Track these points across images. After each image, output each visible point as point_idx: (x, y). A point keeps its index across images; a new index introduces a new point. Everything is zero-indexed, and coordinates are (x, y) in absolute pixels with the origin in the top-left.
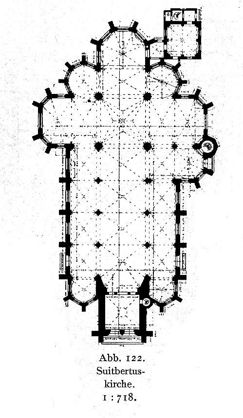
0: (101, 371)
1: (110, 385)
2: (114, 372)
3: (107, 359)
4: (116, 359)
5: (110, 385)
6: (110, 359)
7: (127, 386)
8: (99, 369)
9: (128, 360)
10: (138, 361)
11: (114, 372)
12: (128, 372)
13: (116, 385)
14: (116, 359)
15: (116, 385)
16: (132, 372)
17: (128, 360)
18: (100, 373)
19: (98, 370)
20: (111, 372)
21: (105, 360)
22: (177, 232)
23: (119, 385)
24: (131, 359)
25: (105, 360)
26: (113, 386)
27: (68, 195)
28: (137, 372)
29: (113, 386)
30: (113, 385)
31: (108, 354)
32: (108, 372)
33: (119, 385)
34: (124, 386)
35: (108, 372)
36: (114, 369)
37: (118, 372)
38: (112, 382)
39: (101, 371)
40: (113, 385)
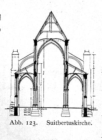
0: (49, 123)
1: (77, 123)
2: (57, 123)
3: (14, 123)
4: (20, 123)
5: (77, 123)
6: (16, 123)
7: (87, 124)
8: (48, 121)
9: (27, 124)
10: (30, 124)
11: (57, 123)
12: (66, 123)
13: (81, 123)
14: (20, 123)
15: (81, 123)
16: (68, 123)
17: (27, 124)
18: (49, 124)
19: (47, 122)
20: (55, 124)
21: (13, 124)
22: (50, 28)
23: (83, 124)
24: (33, 123)
25: (13, 124)
26: (79, 124)
27: (66, 50)
28: (72, 124)
29: (79, 124)
30: (79, 123)
31: (15, 120)
32: (53, 124)
33: (83, 123)
34: (86, 124)
35: (53, 124)
36: (57, 121)
37: (59, 123)
38: (79, 122)
39: (49, 123)
40: (79, 123)
